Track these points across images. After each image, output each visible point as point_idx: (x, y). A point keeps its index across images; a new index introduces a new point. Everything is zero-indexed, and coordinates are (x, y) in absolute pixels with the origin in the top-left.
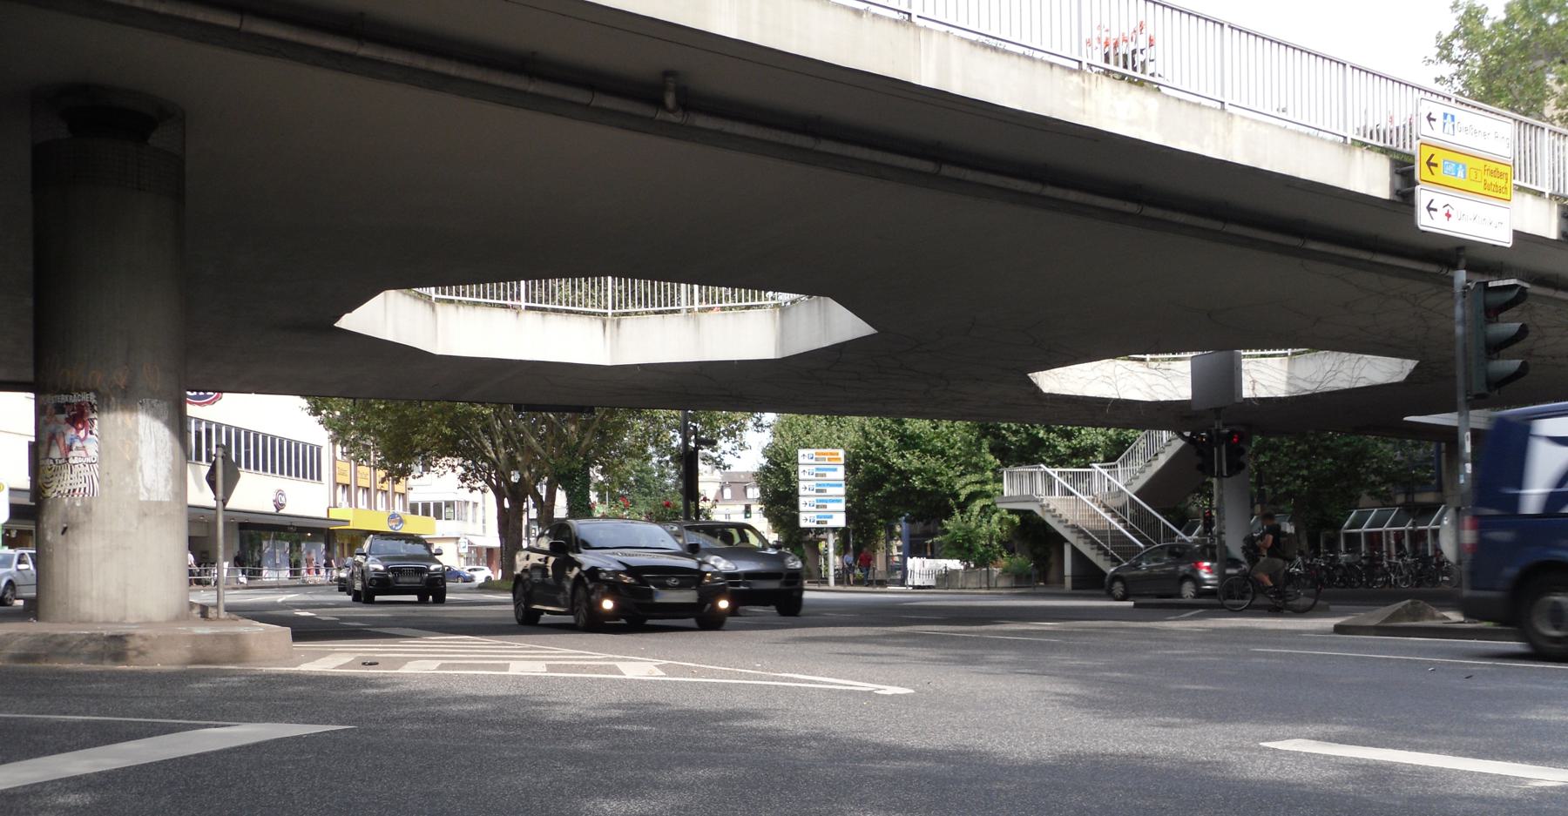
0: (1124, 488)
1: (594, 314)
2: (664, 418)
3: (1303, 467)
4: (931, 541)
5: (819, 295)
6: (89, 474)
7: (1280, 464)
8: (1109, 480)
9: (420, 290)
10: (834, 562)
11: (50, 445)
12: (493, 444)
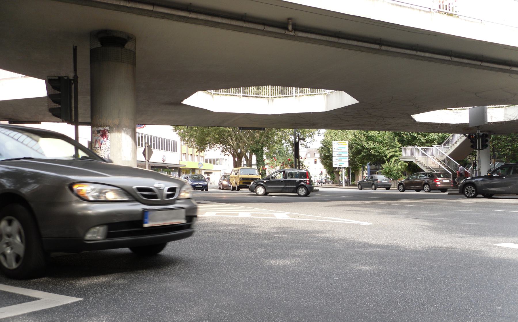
0: (444, 154)
1: (265, 97)
2: (288, 131)
3: (510, 145)
4: (377, 172)
5: (339, 90)
6: (107, 152)
7: (501, 144)
8: (439, 151)
9: (208, 91)
10: (344, 177)
11: (96, 143)
12: (232, 140)
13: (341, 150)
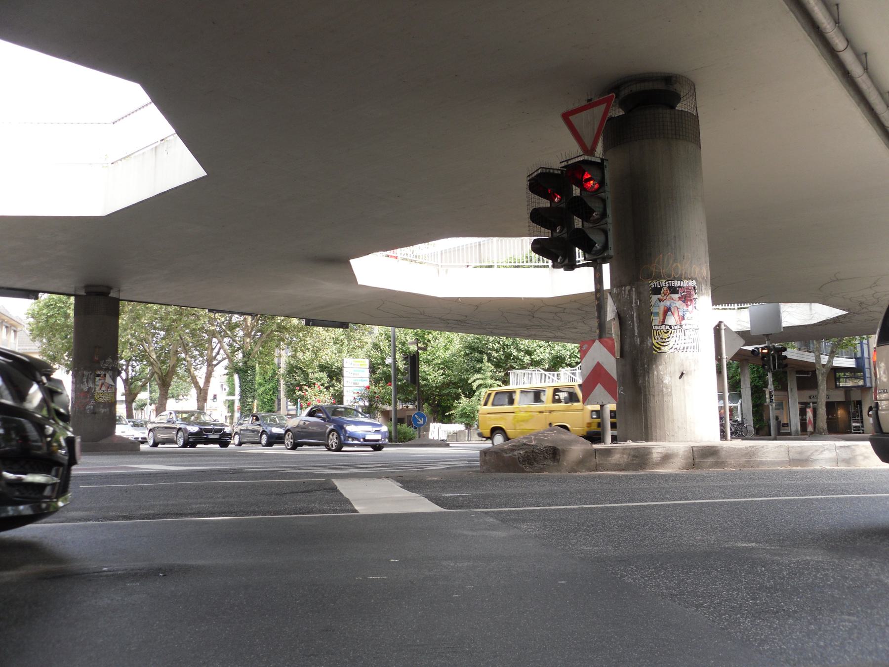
13: (356, 374)
